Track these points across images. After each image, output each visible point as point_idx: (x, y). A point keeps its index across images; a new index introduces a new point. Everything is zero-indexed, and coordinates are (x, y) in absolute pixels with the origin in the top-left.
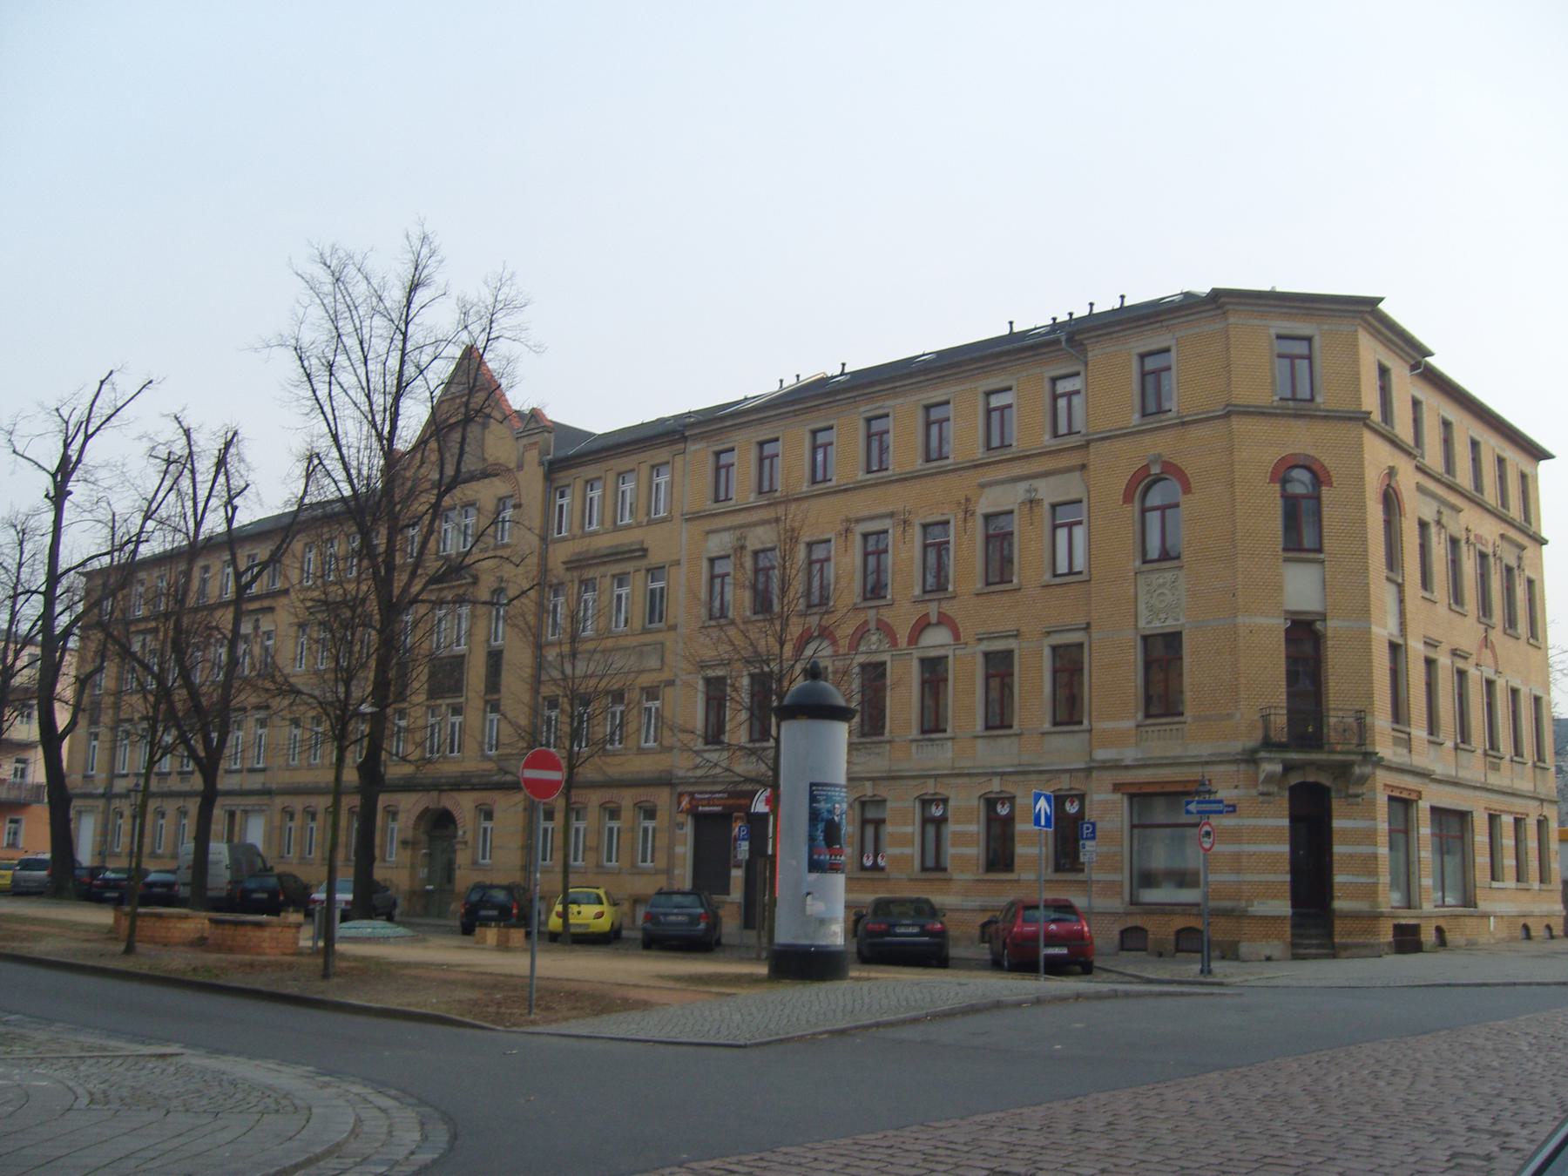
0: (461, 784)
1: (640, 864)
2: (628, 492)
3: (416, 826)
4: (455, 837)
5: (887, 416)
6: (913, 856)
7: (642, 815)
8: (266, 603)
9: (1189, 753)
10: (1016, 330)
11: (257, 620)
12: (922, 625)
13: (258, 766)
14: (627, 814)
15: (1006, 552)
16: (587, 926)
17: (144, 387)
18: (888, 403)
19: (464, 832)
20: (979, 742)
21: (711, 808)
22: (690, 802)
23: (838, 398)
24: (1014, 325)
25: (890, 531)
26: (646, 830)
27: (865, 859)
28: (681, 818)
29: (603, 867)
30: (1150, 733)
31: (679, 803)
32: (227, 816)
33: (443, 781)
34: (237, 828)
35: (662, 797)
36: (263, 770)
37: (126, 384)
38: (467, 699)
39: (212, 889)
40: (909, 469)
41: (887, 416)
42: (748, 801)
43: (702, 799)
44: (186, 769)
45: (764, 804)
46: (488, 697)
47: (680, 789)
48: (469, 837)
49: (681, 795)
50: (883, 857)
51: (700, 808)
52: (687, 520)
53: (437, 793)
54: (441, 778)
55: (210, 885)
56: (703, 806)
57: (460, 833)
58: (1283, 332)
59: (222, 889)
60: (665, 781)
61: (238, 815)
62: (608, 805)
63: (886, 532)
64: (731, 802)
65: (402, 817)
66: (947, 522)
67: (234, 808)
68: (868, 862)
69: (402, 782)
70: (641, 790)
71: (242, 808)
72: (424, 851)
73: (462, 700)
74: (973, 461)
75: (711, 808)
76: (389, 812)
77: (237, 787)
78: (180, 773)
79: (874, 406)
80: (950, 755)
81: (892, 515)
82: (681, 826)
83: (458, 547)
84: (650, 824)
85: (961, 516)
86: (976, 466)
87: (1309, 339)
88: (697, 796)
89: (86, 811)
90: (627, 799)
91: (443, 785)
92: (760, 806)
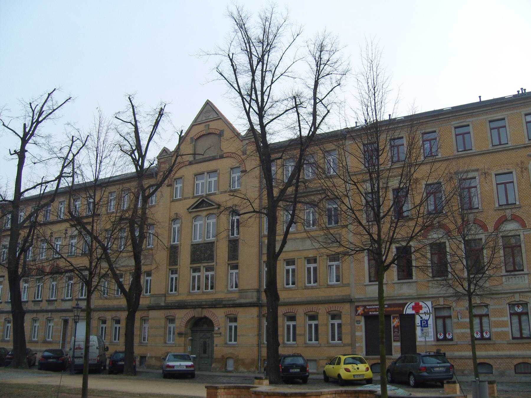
0: (215, 304)
1: (229, 342)
2: (179, 188)
3: (186, 326)
4: (213, 331)
5: (468, 125)
7: (228, 321)
9: (430, 293)
10: (482, 100)
12: (503, 220)
13: (52, 299)
16: (363, 375)
17: (67, 100)
18: (467, 120)
19: (219, 328)
20: (396, 285)
22: (364, 310)
23: (440, 117)
24: (481, 98)
25: (477, 178)
26: (102, 328)
27: (439, 335)
28: (358, 318)
29: (113, 342)
30: (520, 278)
31: (357, 311)
32: (63, 321)
33: (204, 303)
35: (346, 309)
37: (58, 98)
38: (216, 263)
39: (92, 359)
40: (484, 149)
41: (468, 125)
42: (401, 309)
43: (370, 309)
44: (36, 299)
45: (411, 309)
46: (230, 262)
47: (356, 304)
48: (222, 330)
50: (449, 334)
51: (370, 313)
53: (200, 309)
54: (202, 302)
55: (90, 358)
57: (216, 328)
59: (94, 360)
60: (349, 300)
62: (115, 318)
63: (475, 178)
64: (389, 309)
65: (177, 322)
66: (511, 173)
67: (67, 318)
68: (441, 337)
69: (177, 304)
72: (190, 338)
73: (214, 263)
74: (525, 144)
76: (143, 319)
78: (33, 301)
79: (459, 121)
80: (527, 282)
81: (477, 170)
82: (359, 322)
83: (206, 191)
85: (519, 170)
86: (525, 147)
88: (367, 307)
91: (204, 305)
92: (409, 310)
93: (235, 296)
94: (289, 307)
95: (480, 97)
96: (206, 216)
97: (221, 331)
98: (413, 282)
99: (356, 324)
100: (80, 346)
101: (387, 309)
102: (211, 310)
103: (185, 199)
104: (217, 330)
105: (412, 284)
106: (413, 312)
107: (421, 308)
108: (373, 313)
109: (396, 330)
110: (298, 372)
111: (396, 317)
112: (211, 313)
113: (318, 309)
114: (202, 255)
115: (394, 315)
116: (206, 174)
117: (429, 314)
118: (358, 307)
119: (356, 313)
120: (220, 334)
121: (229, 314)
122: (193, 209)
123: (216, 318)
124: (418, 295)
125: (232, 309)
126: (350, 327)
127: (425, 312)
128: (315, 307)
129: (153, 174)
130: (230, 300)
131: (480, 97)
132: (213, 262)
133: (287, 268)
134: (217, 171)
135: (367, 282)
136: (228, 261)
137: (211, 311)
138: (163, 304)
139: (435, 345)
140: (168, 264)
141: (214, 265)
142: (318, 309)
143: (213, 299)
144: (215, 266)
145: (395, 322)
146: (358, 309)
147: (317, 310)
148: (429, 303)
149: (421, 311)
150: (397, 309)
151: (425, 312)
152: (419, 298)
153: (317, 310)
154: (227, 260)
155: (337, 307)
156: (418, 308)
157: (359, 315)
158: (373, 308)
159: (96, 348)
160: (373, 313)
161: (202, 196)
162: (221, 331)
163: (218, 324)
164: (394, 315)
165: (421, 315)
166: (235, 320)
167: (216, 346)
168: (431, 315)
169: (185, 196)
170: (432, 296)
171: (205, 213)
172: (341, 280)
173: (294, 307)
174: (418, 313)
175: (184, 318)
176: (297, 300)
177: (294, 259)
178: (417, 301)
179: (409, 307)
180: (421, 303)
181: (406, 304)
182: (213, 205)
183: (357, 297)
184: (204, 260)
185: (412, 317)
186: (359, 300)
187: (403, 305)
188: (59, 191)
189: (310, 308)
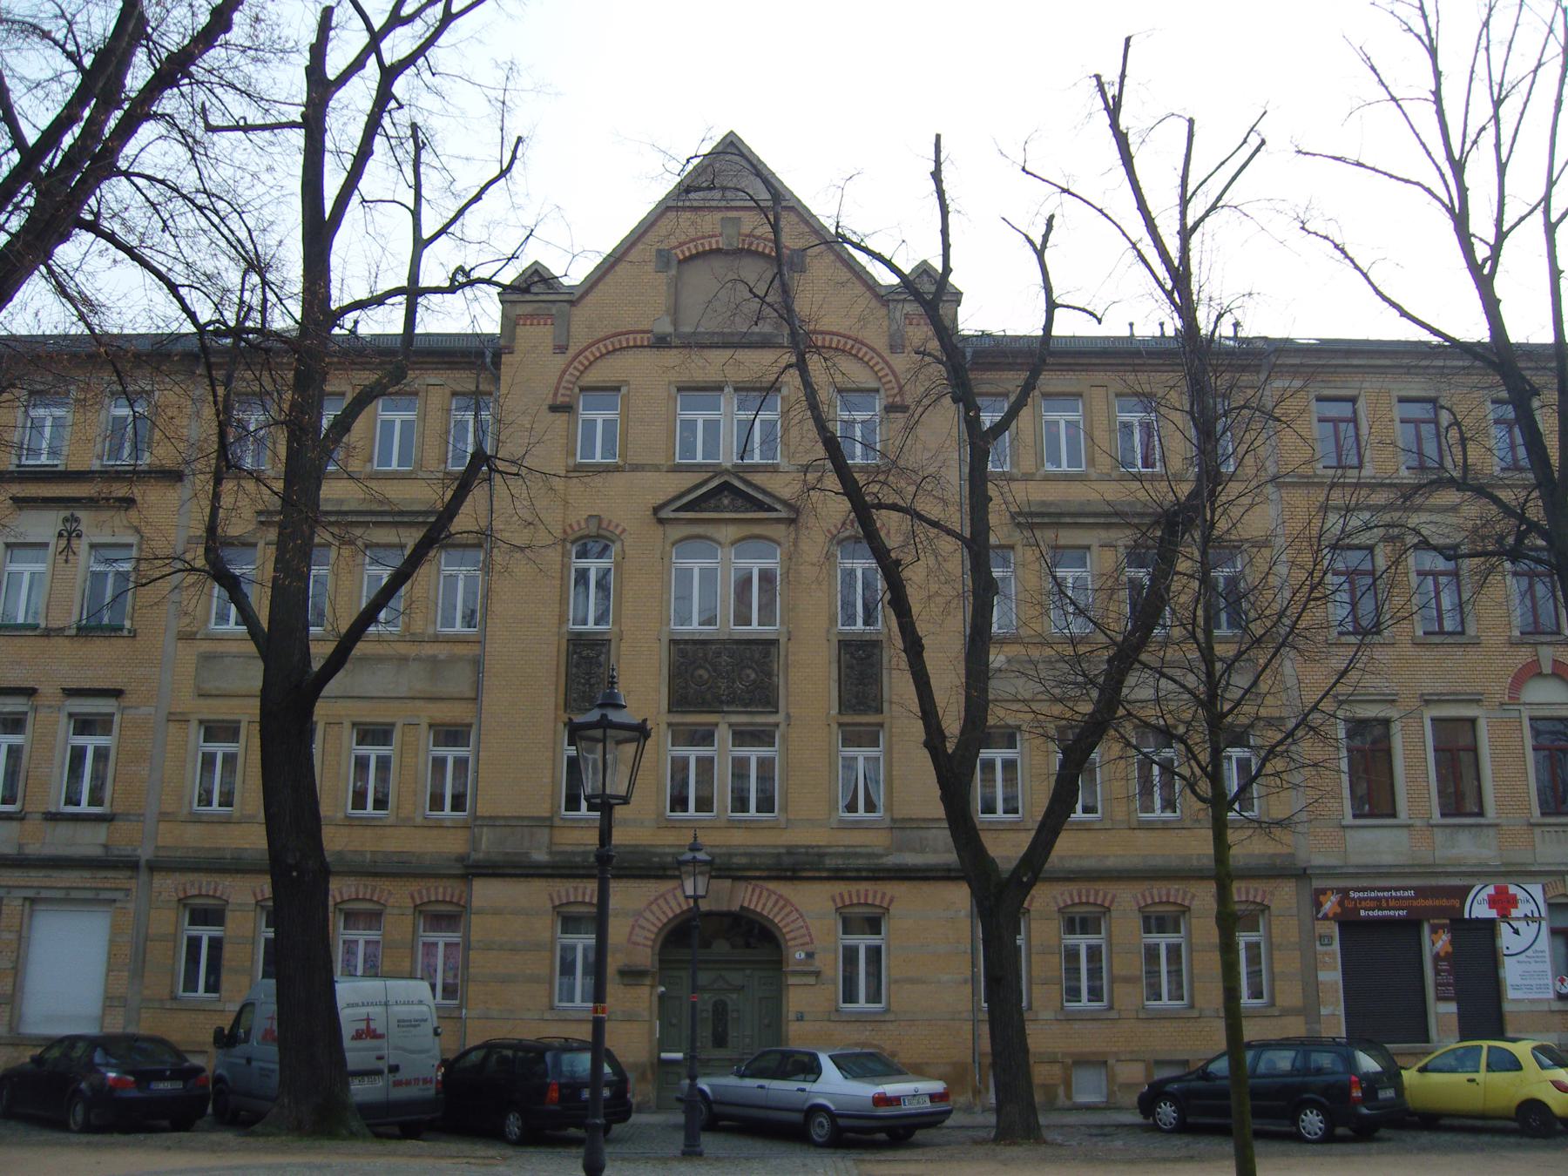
8: (120, 490)
19: (810, 955)
21: (1386, 913)
22: (1341, 903)
31: (1319, 905)
38: (788, 716)
46: (846, 719)
47: (1317, 884)
53: (728, 883)
56: (1365, 909)
58: (1404, 393)
59: (425, 1081)
64: (1421, 902)
70: (1083, 886)
75: (1386, 913)
87: (1353, 400)
88: (1352, 894)
90: (1126, 900)
92: (1479, 909)
93: (875, 841)
94: (1084, 886)
95: (1131, 325)
96: (732, 544)
97: (818, 963)
98: (1489, 826)
99: (1319, 948)
100: (373, 1025)
101: (1415, 903)
102: (772, 885)
103: (636, 468)
104: (800, 962)
105: (1485, 830)
106: (1493, 914)
107: (1513, 901)
108: (1371, 913)
109: (1444, 965)
110: (1391, 1099)
111: (1442, 927)
112: (774, 898)
113: (1189, 896)
114: (723, 684)
115: (1436, 921)
116: (728, 390)
117: (1538, 920)
118: (1324, 891)
119: (1318, 912)
120: (817, 974)
121: (568, 904)
122: (776, 510)
123: (795, 915)
124: (1504, 864)
125: (863, 886)
126: (1297, 954)
127: (1526, 916)
128: (1178, 890)
129: (481, 354)
130: (856, 855)
131: (1131, 325)
132: (777, 712)
133: (206, 750)
134: (618, 389)
135: (1349, 819)
136: (840, 712)
137: (771, 892)
138: (540, 856)
139: (1559, 1011)
140: (562, 702)
141: (777, 725)
142: (1189, 896)
143: (775, 847)
144: (782, 726)
145: (1436, 943)
146: (1322, 898)
147: (1183, 899)
148: (1536, 890)
149: (1514, 913)
150: (1444, 902)
151: (1526, 916)
152: (1508, 874)
153: (1183, 899)
154: (834, 711)
155: (1252, 892)
156: (1503, 902)
157: (1325, 917)
158: (1372, 899)
159: (431, 1031)
160: (1371, 913)
161: (717, 471)
162: (818, 963)
163: (807, 939)
164: (1436, 921)
165: (1514, 924)
166: (873, 924)
167: (800, 1018)
168: (1543, 923)
169: (634, 459)
170: (1547, 868)
171: (730, 532)
172: (20, 795)
173: (1100, 886)
174: (1505, 916)
175: (648, 915)
176: (1110, 863)
177: (239, 722)
178: (1501, 882)
179: (1479, 897)
180: (1513, 889)
181: (1470, 888)
182: (771, 509)
183: (1318, 860)
184: (728, 703)
185: (1489, 926)
186: (1329, 872)
187: (1465, 891)
188: (417, 344)
189: (1159, 890)
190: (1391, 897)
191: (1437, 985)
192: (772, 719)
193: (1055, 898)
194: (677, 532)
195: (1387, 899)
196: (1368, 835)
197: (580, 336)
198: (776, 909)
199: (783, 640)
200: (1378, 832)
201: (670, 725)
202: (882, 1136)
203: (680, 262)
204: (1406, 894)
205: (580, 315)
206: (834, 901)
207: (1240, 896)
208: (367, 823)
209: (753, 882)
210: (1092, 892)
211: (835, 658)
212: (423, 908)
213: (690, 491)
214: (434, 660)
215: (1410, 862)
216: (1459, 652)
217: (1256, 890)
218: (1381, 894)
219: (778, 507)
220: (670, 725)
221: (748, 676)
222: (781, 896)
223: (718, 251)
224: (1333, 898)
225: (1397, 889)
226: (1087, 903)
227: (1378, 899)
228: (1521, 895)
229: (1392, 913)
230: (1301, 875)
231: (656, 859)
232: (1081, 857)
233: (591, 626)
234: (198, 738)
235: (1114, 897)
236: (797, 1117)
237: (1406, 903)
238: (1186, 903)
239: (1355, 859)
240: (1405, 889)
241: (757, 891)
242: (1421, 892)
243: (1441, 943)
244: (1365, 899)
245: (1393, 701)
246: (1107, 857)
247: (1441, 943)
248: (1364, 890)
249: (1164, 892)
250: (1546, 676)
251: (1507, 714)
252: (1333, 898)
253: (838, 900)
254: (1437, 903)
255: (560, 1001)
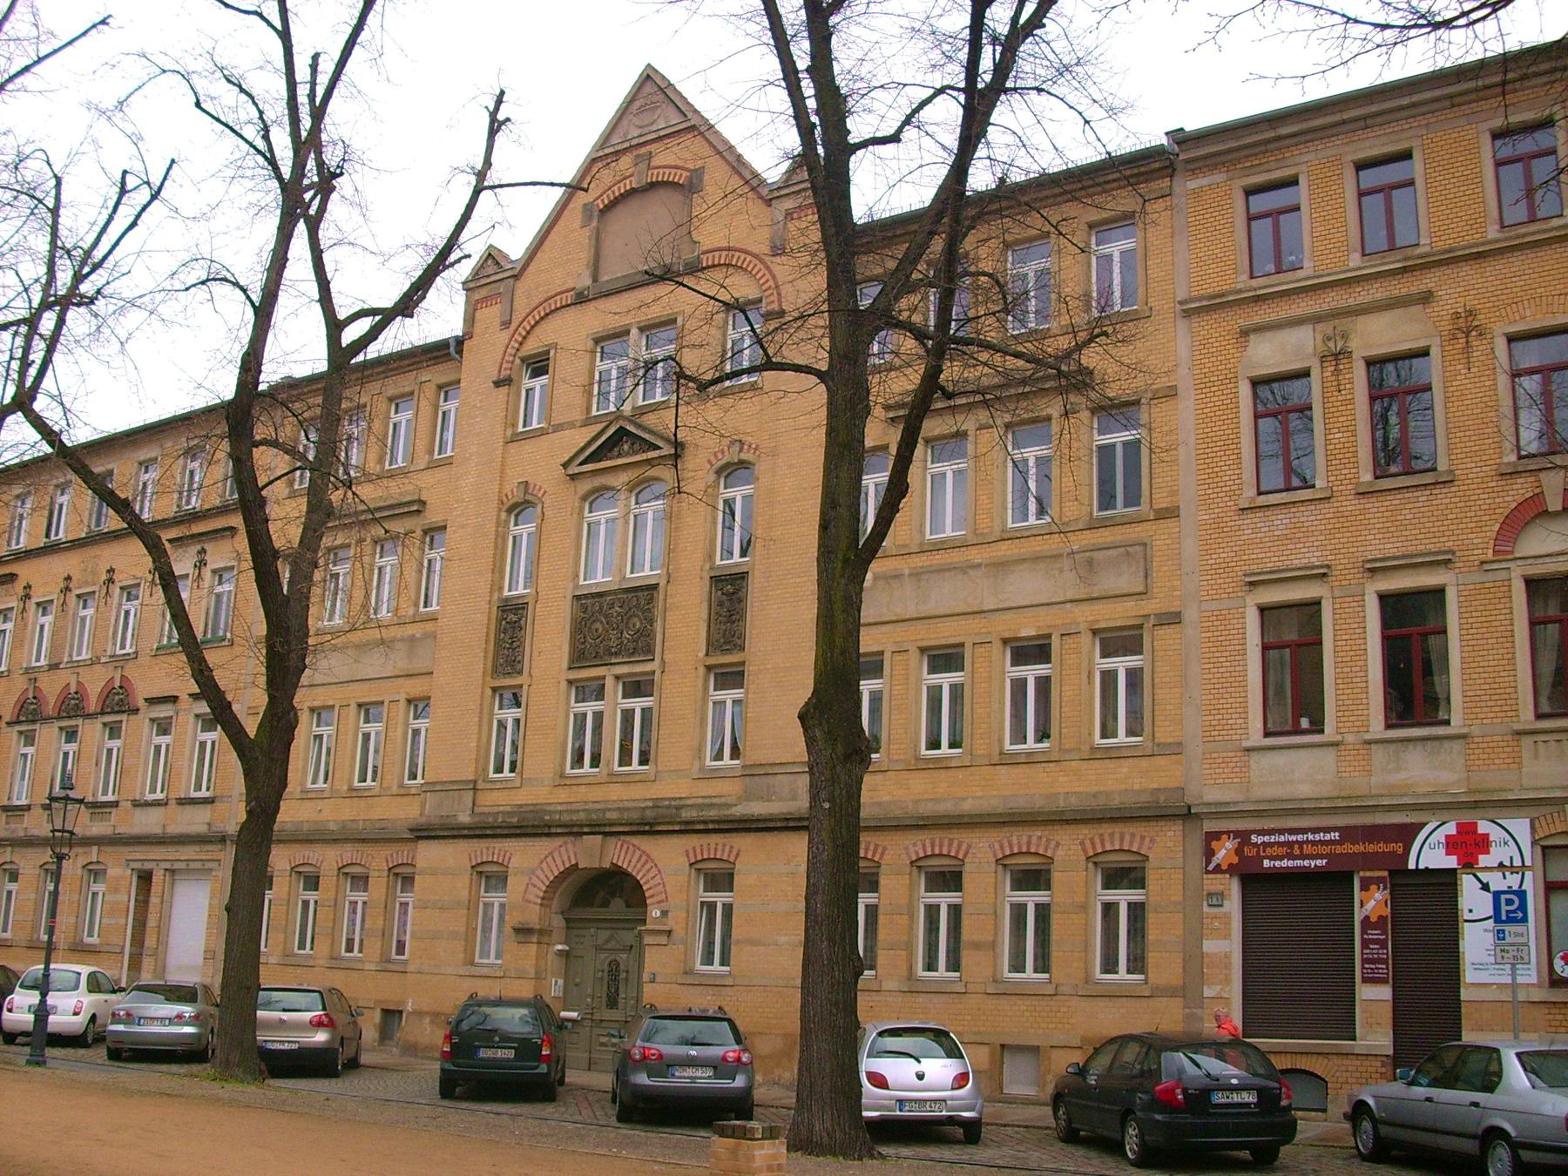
3: (546, 899)
6: (1227, 956)
11: (203, 551)
13: (104, 799)
14: (378, 886)
15: (1394, 433)
19: (665, 913)
21: (1298, 863)
31: (1209, 854)
34: (154, 900)
36: (209, 801)
46: (711, 661)
47: (1210, 826)
49: (1214, 836)
52: (1188, 314)
56: (1272, 858)
61: (157, 878)
62: (300, 869)
64: (1349, 848)
67: (148, 866)
70: (936, 835)
71: (168, 865)
72: (559, 947)
75: (1298, 863)
77: (158, 830)
84: (312, 896)
88: (1254, 838)
89: (188, 871)
92: (1430, 854)
99: (1206, 909)
101: (1339, 849)
102: (636, 840)
105: (1447, 744)
106: (1451, 862)
107: (1483, 844)
108: (1277, 864)
113: (1052, 845)
115: (1368, 874)
118: (1216, 836)
119: (1208, 862)
122: (660, 448)
123: (654, 871)
138: (465, 818)
142: (1052, 845)
145: (1371, 903)
148: (1520, 827)
149: (1484, 860)
150: (1380, 847)
151: (1501, 865)
152: (1476, 805)
155: (1127, 838)
156: (1468, 845)
160: (1277, 864)
164: (1368, 874)
165: (1483, 876)
168: (1528, 875)
173: (956, 835)
174: (1469, 864)
176: (968, 806)
177: (962, 645)
178: (1467, 817)
180: (1483, 827)
183: (1213, 795)
189: (1018, 839)
190: (1308, 842)
191: (1364, 961)
192: (648, 667)
193: (906, 848)
194: (585, 486)
195: (1301, 844)
196: (1279, 759)
197: (522, 306)
198: (639, 865)
199: (663, 583)
200: (1294, 755)
201: (570, 682)
202: (1245, 1154)
203: (601, 211)
204: (1328, 837)
205: (522, 286)
206: (688, 856)
207: (1112, 843)
208: (942, 765)
209: (622, 838)
210: (946, 842)
211: (706, 597)
212: (1007, 862)
213: (589, 444)
214: (412, 638)
215: (1335, 794)
216: (1423, 496)
217: (1133, 835)
218: (1293, 838)
219: (660, 444)
220: (570, 682)
221: (634, 625)
222: (644, 852)
223: (633, 192)
224: (1229, 845)
225: (1315, 831)
226: (941, 855)
227: (1290, 844)
228: (1495, 833)
229: (1306, 863)
230: (1187, 815)
231: (547, 818)
232: (936, 800)
233: (736, 558)
234: (921, 668)
235: (969, 847)
236: (1470, 1146)
237: (1326, 850)
238: (1049, 854)
239: (1258, 793)
240: (1327, 830)
241: (625, 846)
242: (1348, 833)
243: (1373, 903)
244: (1271, 845)
245: (1324, 575)
246: (964, 799)
247: (1373, 903)
248: (1270, 832)
249: (1025, 839)
250: (1556, 514)
251: (1490, 576)
252: (1229, 845)
253: (691, 855)
254: (1371, 848)
255: (481, 958)
